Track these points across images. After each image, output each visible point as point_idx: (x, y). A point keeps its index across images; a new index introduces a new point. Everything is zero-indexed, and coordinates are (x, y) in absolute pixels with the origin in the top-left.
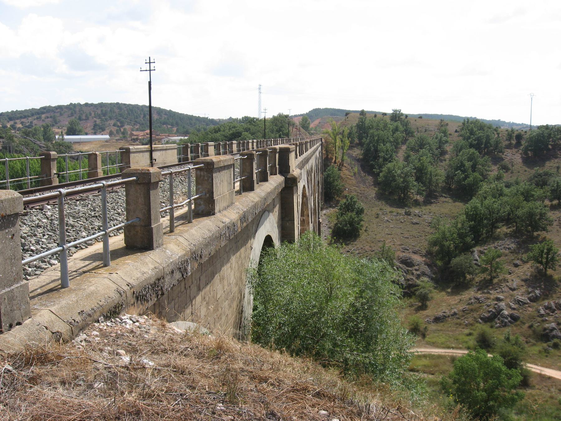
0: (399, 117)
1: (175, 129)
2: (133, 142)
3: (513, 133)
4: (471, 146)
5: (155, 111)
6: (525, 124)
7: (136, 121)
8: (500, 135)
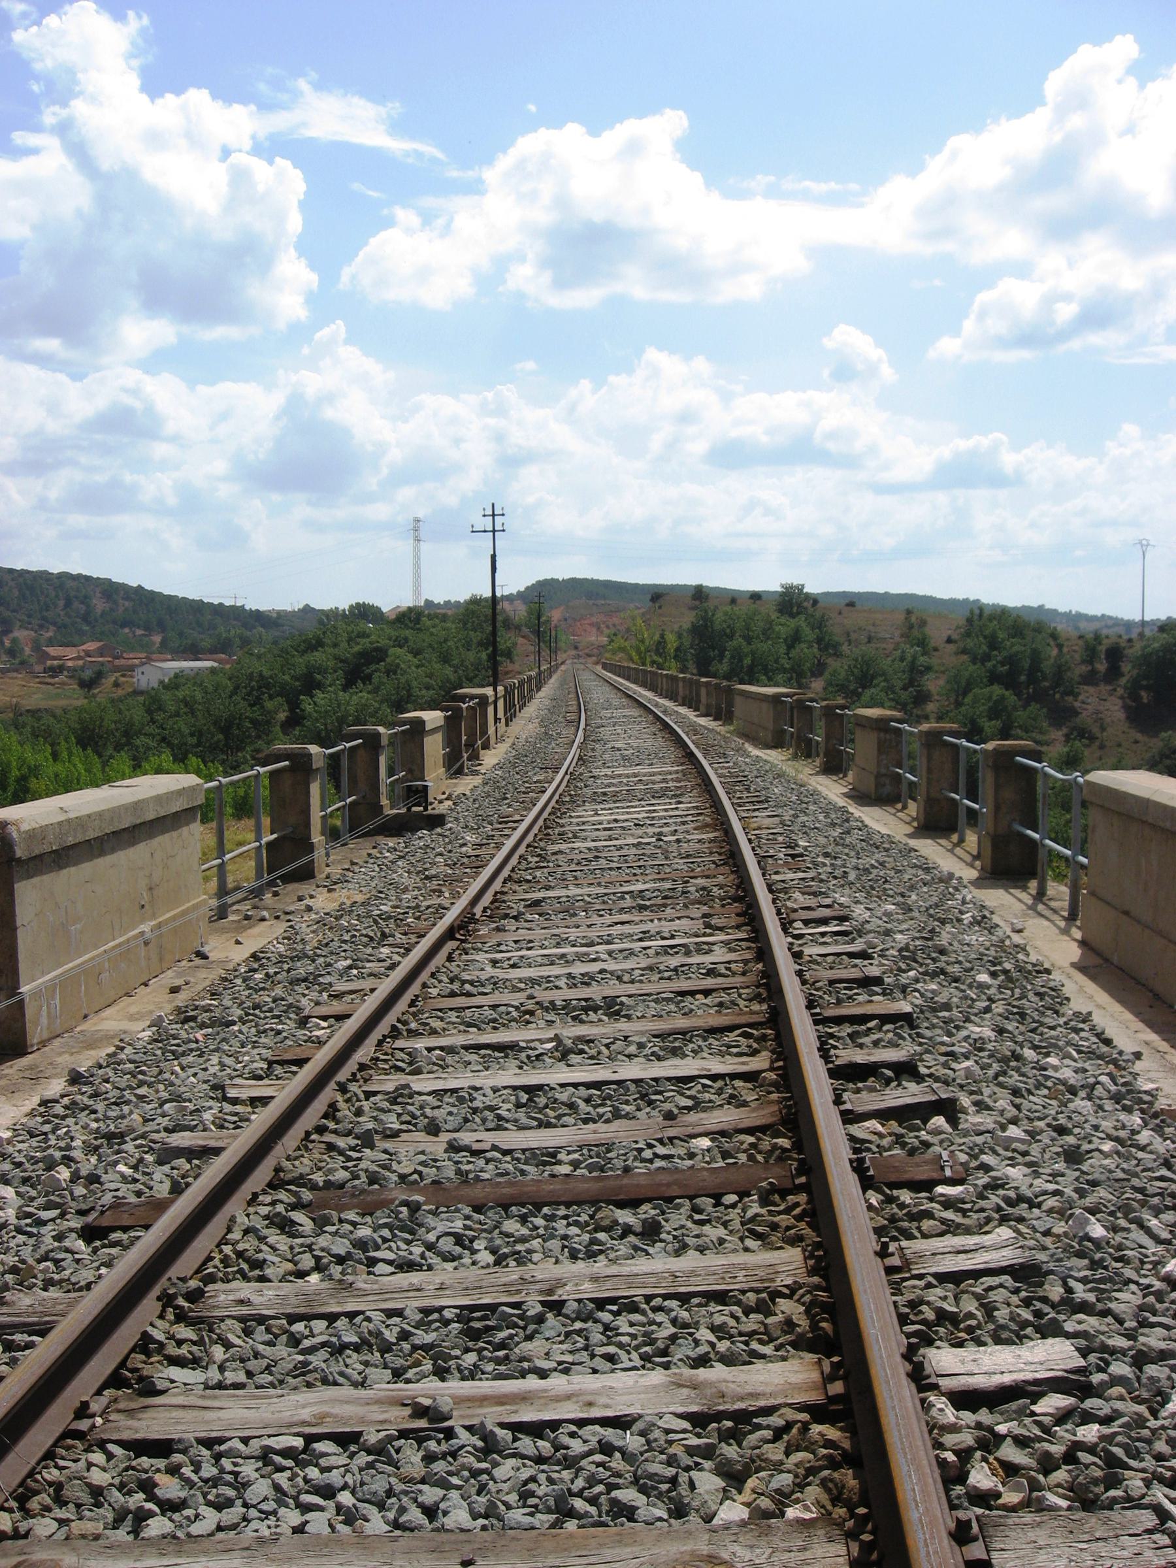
0: (799, 605)
1: (157, 639)
2: (50, 676)
3: (1100, 644)
4: (994, 678)
5: (98, 590)
6: (1110, 618)
7: (44, 618)
8: (1065, 650)
